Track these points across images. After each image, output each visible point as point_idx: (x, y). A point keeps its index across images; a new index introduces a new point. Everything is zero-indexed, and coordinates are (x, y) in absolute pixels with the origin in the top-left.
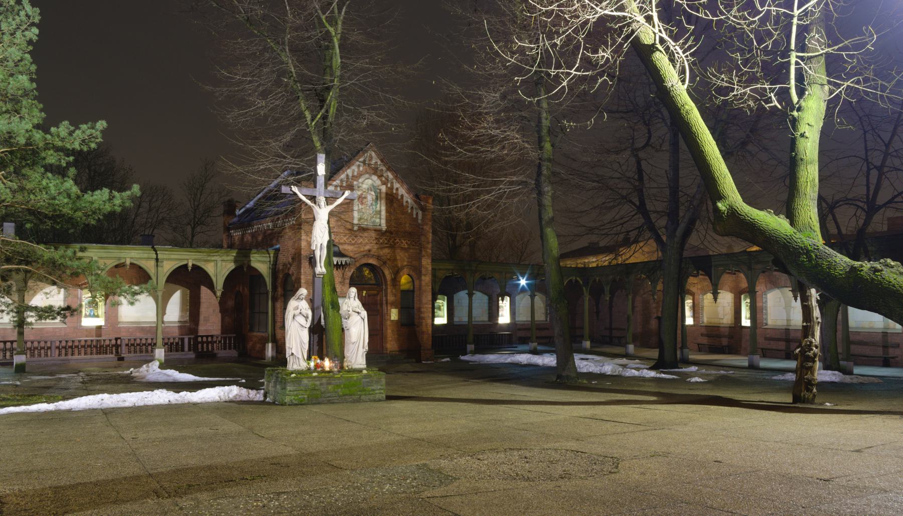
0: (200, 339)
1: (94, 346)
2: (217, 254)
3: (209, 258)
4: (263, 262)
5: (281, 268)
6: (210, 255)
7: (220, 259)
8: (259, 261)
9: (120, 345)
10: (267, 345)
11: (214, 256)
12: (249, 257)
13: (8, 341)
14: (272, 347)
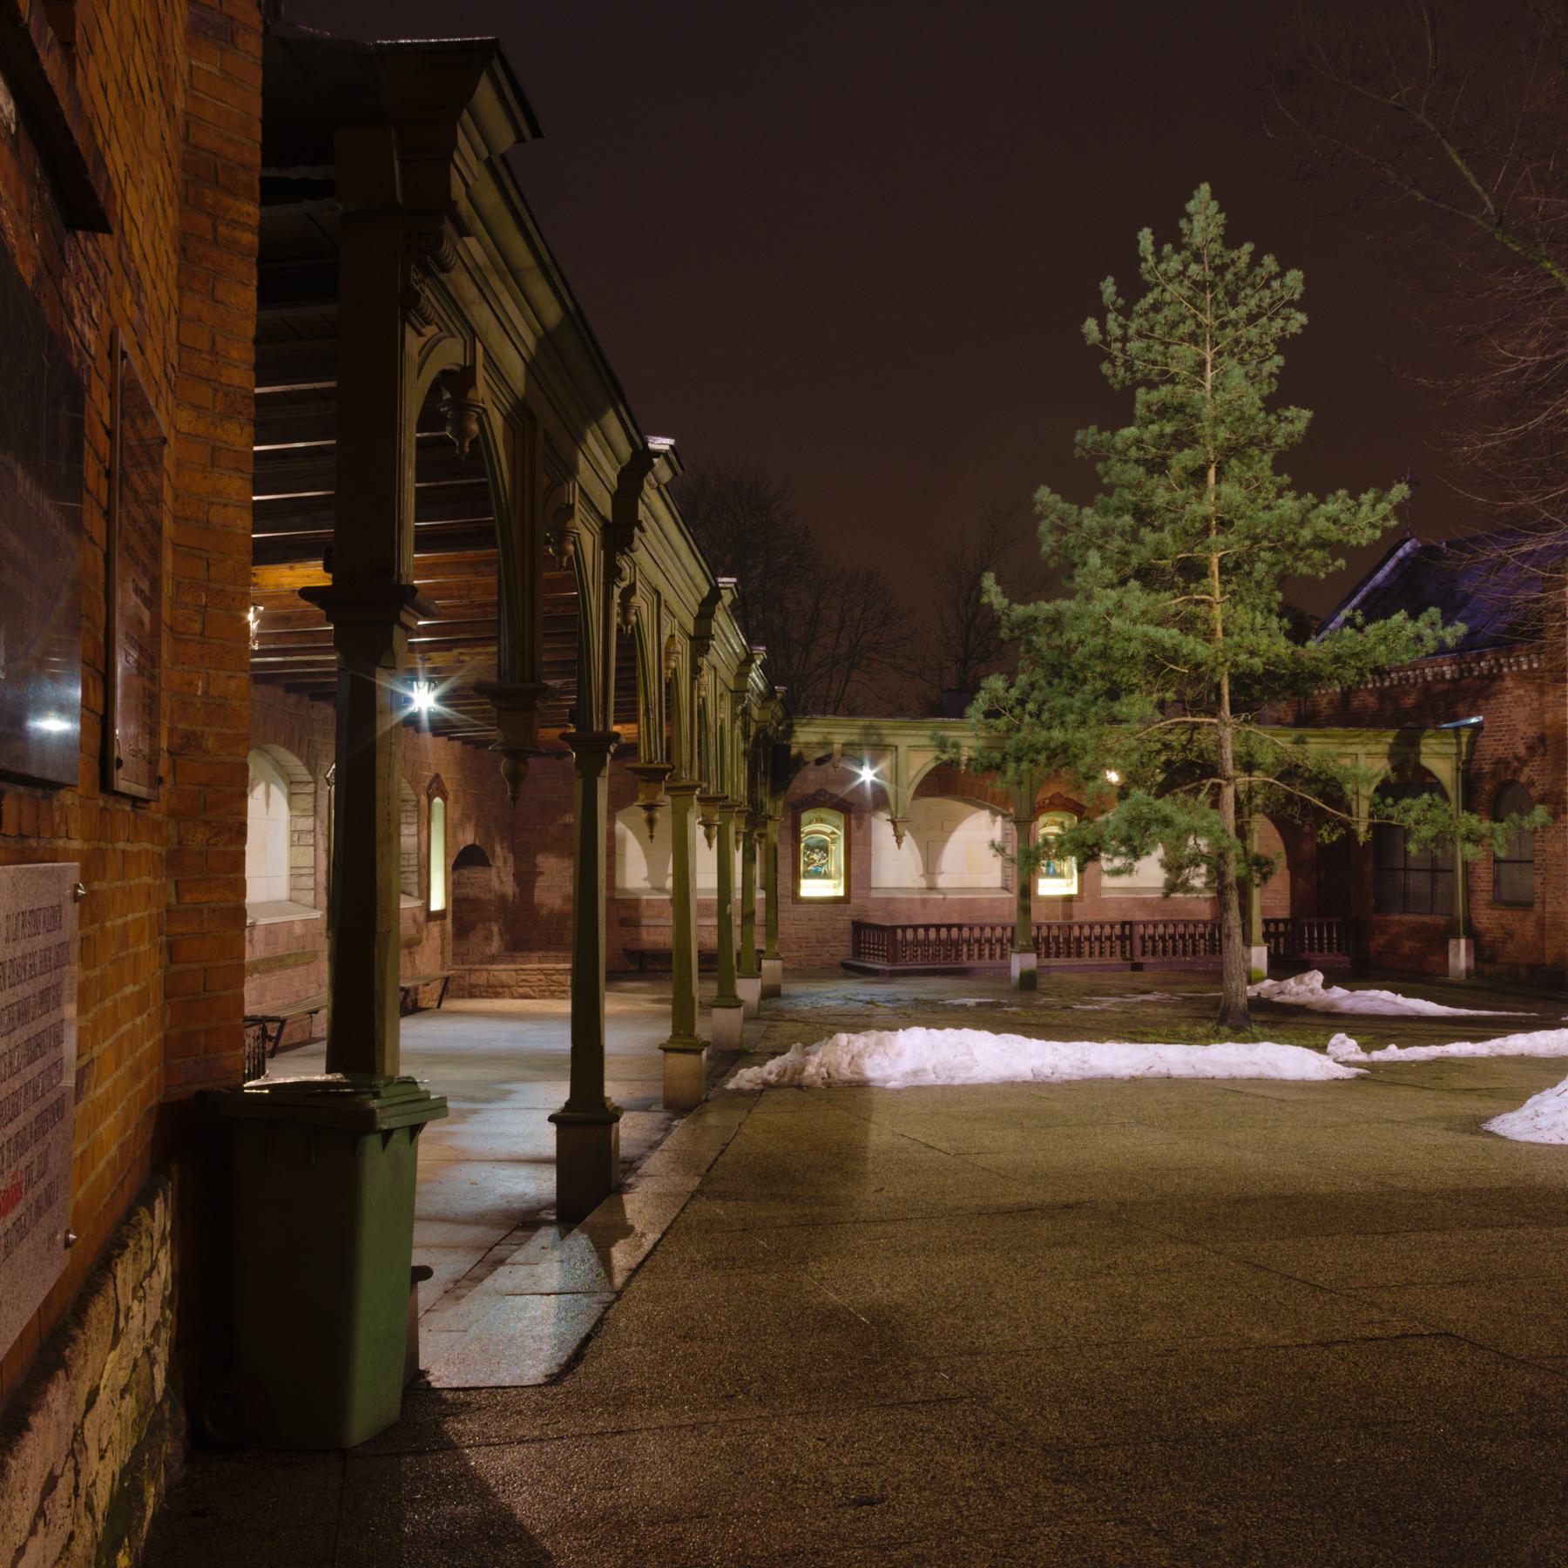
0: (1076, 932)
1: (1160, 937)
2: (1357, 740)
3: (1343, 750)
4: (1444, 756)
5: (1487, 768)
6: (1344, 744)
7: (1364, 750)
8: (1437, 753)
9: (1130, 938)
10: (1452, 942)
11: (1351, 744)
12: (1417, 744)
13: (921, 926)
14: (1467, 949)
